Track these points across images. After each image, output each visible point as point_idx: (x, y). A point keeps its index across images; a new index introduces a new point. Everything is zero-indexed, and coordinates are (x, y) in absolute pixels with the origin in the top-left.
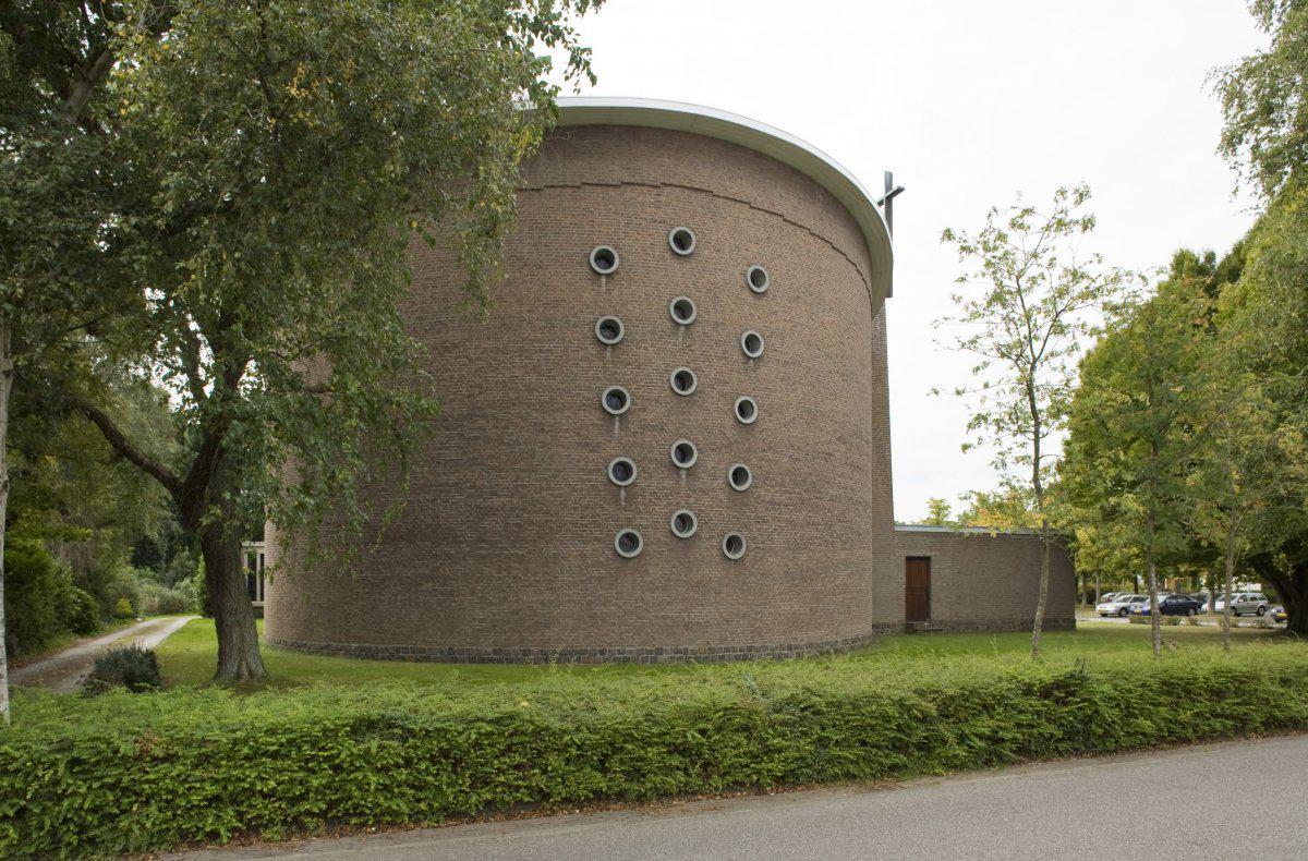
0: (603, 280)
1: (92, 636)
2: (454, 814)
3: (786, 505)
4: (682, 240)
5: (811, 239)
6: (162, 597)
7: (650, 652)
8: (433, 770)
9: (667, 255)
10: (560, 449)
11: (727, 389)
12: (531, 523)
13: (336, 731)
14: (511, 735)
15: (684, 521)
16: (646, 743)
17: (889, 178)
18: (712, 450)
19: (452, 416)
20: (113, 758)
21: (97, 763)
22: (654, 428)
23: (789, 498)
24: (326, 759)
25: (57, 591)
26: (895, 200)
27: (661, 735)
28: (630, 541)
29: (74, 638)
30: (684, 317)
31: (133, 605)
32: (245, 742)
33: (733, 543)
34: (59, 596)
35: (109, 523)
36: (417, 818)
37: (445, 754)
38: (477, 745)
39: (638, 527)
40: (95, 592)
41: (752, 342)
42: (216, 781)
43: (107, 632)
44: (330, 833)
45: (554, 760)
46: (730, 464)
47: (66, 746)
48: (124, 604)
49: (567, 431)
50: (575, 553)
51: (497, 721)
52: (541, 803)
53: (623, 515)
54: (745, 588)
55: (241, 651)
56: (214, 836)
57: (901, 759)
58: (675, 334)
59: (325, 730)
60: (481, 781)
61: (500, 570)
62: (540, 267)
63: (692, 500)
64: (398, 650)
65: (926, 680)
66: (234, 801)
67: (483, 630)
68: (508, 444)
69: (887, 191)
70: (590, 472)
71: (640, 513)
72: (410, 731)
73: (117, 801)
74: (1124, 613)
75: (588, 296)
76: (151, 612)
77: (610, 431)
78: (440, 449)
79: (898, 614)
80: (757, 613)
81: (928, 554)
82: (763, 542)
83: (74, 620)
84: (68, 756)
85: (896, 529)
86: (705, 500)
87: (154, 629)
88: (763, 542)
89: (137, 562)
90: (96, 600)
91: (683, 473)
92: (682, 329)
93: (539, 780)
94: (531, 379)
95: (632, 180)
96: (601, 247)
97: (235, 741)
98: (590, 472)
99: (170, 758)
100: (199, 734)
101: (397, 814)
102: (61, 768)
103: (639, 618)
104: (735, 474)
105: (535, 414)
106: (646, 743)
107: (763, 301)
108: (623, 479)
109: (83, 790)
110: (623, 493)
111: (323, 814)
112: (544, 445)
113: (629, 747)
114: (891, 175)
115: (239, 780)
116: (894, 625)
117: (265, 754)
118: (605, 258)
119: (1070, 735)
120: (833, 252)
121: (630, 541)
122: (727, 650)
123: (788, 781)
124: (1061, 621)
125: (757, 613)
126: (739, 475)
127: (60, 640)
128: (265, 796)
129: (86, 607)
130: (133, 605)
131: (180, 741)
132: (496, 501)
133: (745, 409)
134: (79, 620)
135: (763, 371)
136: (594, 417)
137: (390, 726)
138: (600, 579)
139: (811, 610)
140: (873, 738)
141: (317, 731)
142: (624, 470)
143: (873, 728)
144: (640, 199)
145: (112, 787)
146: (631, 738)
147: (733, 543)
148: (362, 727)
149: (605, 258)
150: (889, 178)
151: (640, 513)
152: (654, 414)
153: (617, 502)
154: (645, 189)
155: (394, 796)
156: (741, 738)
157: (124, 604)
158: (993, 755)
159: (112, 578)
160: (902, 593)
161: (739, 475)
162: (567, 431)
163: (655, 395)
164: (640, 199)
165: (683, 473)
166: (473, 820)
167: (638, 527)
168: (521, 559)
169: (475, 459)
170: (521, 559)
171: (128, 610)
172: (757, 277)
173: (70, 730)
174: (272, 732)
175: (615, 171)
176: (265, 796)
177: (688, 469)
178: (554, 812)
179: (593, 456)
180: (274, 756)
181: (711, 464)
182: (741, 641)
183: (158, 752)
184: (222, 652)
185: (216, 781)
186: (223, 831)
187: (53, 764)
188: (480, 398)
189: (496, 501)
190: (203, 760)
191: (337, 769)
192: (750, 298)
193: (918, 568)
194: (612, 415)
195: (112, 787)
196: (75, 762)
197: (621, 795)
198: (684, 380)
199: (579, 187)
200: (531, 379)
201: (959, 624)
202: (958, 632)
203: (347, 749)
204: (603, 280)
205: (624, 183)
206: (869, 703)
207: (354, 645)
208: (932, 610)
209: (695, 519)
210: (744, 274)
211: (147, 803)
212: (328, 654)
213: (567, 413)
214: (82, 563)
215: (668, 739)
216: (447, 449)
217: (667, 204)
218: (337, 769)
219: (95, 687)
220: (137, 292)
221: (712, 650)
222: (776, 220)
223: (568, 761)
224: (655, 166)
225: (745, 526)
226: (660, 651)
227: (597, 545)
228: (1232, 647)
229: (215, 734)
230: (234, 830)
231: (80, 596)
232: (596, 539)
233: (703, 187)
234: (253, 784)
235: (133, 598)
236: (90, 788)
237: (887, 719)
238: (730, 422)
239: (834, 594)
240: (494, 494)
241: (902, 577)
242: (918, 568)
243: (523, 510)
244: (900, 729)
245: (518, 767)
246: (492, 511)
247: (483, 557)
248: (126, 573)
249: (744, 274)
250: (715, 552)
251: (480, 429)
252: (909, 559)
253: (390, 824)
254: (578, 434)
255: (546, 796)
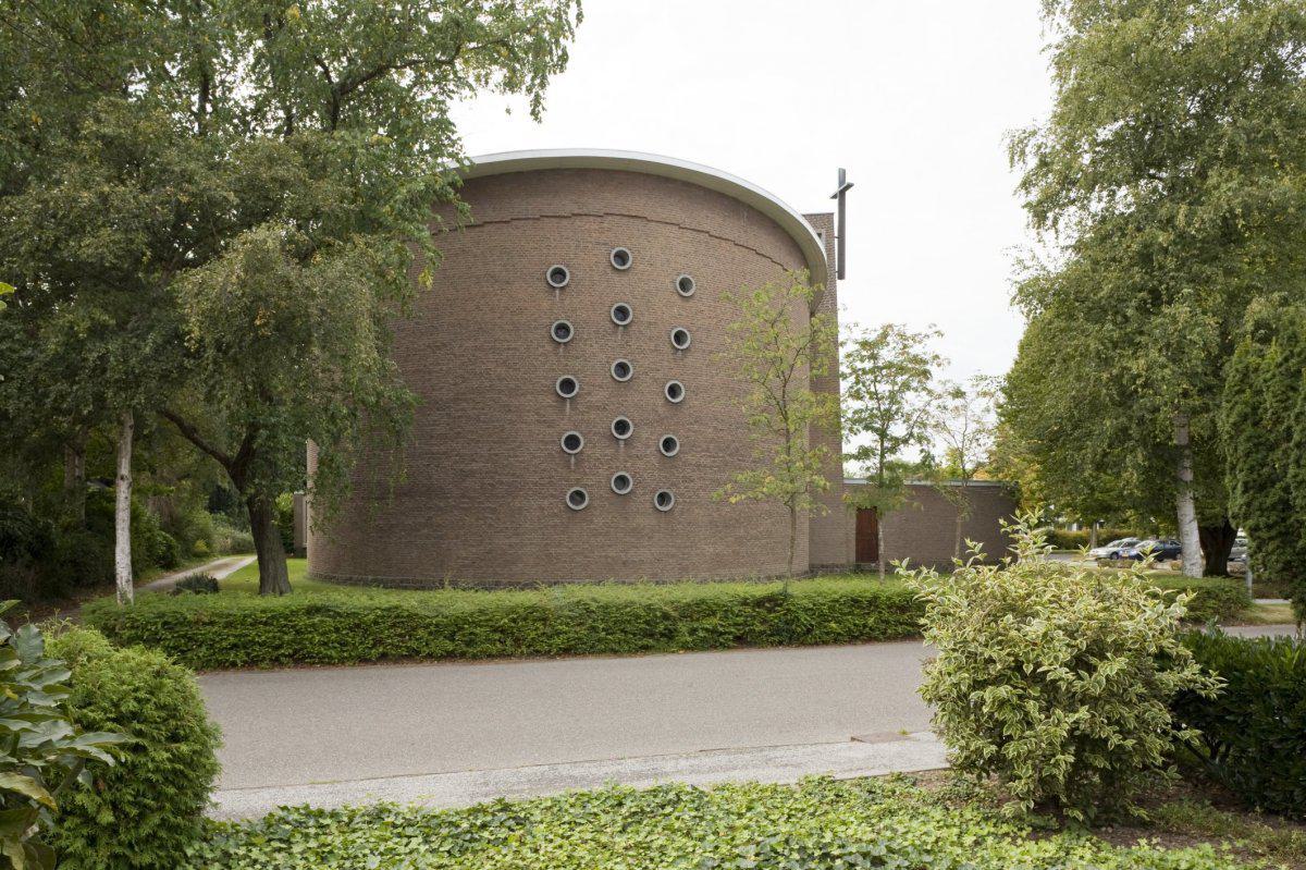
0: (557, 292)
1: (176, 571)
2: (364, 660)
3: (711, 467)
4: (621, 257)
5: (735, 249)
6: (233, 538)
8: (350, 634)
9: (609, 270)
10: (524, 426)
11: (659, 375)
12: (502, 483)
13: (297, 612)
14: (396, 617)
15: (622, 481)
16: (478, 624)
17: (842, 174)
18: (646, 424)
19: (441, 400)
20: (184, 622)
21: (176, 624)
22: (598, 408)
23: (714, 462)
24: (292, 627)
25: (148, 534)
26: (847, 193)
27: (487, 621)
28: (578, 497)
29: (160, 572)
30: (625, 318)
31: (208, 545)
32: (250, 616)
33: (663, 498)
34: (149, 539)
35: (187, 476)
36: (342, 661)
37: (358, 626)
38: (376, 623)
39: (585, 486)
40: (176, 535)
41: (680, 337)
42: (236, 636)
43: (187, 568)
44: (296, 667)
45: (421, 632)
46: (661, 435)
47: (161, 615)
48: (201, 545)
49: (528, 411)
50: (535, 506)
51: (389, 610)
52: (412, 656)
53: (573, 476)
55: (275, 578)
56: (234, 665)
57: (651, 642)
58: (615, 333)
59: (292, 611)
60: (378, 642)
61: (477, 520)
62: (508, 283)
63: (629, 464)
64: (402, 582)
65: (669, 598)
66: (245, 648)
67: (464, 566)
68: (484, 422)
69: (840, 185)
70: (547, 443)
71: (586, 474)
72: (339, 614)
73: (186, 644)
74: (1115, 557)
75: (545, 305)
76: (225, 552)
77: (562, 411)
78: (433, 425)
79: (848, 554)
82: (690, 497)
83: (160, 558)
84: (162, 620)
85: (846, 482)
86: (640, 464)
87: (226, 566)
88: (690, 497)
89: (213, 508)
90: (177, 540)
91: (622, 443)
92: (621, 328)
93: (413, 644)
94: (501, 370)
95: (580, 212)
96: (556, 266)
97: (245, 616)
98: (547, 443)
99: (212, 623)
100: (226, 612)
101: (330, 657)
102: (159, 626)
103: (586, 557)
104: (664, 445)
105: (505, 399)
106: (478, 624)
107: (691, 303)
108: (621, 433)
109: (170, 637)
110: (573, 460)
111: (290, 656)
112: (512, 422)
113: (466, 626)
114: (844, 171)
115: (247, 635)
117: (260, 623)
118: (559, 274)
119: (776, 632)
120: (759, 258)
121: (578, 497)
123: (568, 651)
126: (669, 444)
127: (151, 573)
128: (260, 645)
129: (170, 547)
130: (208, 545)
131: (217, 615)
132: (475, 466)
133: (674, 391)
134: (164, 558)
135: (690, 360)
136: (550, 400)
137: (329, 611)
138: (555, 526)
139: (733, 552)
140: (629, 628)
141: (287, 612)
142: (572, 442)
143: (629, 622)
144: (587, 227)
145: (184, 636)
146: (465, 621)
147: (663, 498)
148: (312, 611)
149: (559, 274)
150: (842, 174)
151: (586, 474)
152: (598, 397)
153: (569, 467)
154: (591, 219)
155: (330, 648)
156: (538, 624)
157: (201, 545)
158: (713, 641)
159: (190, 523)
160: (853, 536)
161: (669, 444)
162: (528, 411)
163: (599, 381)
164: (587, 227)
165: (622, 443)
166: (375, 664)
167: (585, 486)
168: (494, 511)
169: (459, 433)
170: (494, 511)
171: (205, 548)
172: (685, 284)
173: (163, 608)
174: (263, 611)
175: (566, 205)
176: (260, 645)
177: (625, 440)
178: (421, 662)
179: (551, 431)
180: (266, 624)
181: (645, 435)
183: (206, 620)
184: (262, 579)
185: (236, 636)
186: (238, 661)
187: (156, 623)
188: (463, 386)
189: (475, 466)
190: (229, 625)
191: (298, 632)
192: (679, 302)
193: (867, 520)
194: (564, 399)
195: (184, 636)
196: (165, 623)
197: (463, 655)
198: (622, 369)
199: (538, 219)
200: (501, 370)
203: (302, 621)
204: (557, 292)
205: (574, 215)
206: (626, 607)
207: (370, 578)
209: (631, 480)
210: (673, 282)
211: (200, 646)
212: (351, 585)
213: (529, 397)
214: (166, 510)
215: (490, 623)
216: (438, 425)
217: (609, 230)
218: (298, 632)
219: (177, 592)
222: (702, 236)
223: (430, 633)
224: (598, 200)
225: (674, 484)
227: (551, 500)
229: (235, 611)
230: (245, 662)
231: (165, 538)
232: (552, 496)
233: (639, 215)
234: (254, 638)
235: (206, 536)
236: (173, 637)
237: (638, 617)
238: (661, 402)
239: (756, 538)
240: (474, 460)
241: (853, 522)
242: (867, 520)
243: (496, 472)
244: (647, 622)
245: (400, 635)
246: (472, 473)
247: (464, 509)
248: (203, 517)
249: (673, 282)
250: (648, 505)
251: (463, 409)
253: (329, 663)
254: (537, 414)
255: (418, 653)
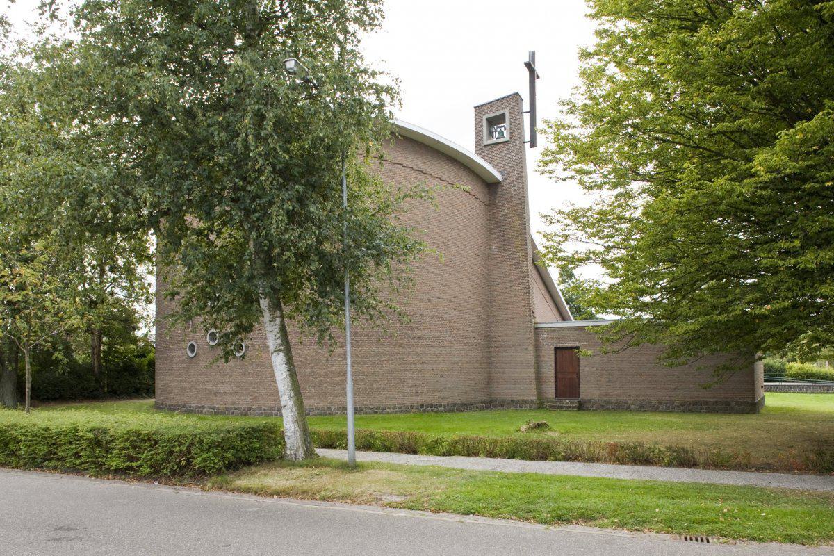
7: (200, 407)
54: (247, 373)
80: (254, 388)
81: (577, 344)
103: (196, 389)
116: (532, 401)
122: (235, 409)
124: (733, 404)
125: (254, 388)
182: (243, 404)
201: (607, 403)
202: (607, 410)
208: (581, 391)
220: (714, 122)
221: (227, 408)
226: (203, 407)
228: (31, 411)
252: (556, 349)
